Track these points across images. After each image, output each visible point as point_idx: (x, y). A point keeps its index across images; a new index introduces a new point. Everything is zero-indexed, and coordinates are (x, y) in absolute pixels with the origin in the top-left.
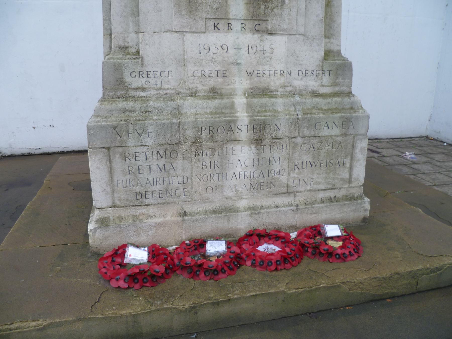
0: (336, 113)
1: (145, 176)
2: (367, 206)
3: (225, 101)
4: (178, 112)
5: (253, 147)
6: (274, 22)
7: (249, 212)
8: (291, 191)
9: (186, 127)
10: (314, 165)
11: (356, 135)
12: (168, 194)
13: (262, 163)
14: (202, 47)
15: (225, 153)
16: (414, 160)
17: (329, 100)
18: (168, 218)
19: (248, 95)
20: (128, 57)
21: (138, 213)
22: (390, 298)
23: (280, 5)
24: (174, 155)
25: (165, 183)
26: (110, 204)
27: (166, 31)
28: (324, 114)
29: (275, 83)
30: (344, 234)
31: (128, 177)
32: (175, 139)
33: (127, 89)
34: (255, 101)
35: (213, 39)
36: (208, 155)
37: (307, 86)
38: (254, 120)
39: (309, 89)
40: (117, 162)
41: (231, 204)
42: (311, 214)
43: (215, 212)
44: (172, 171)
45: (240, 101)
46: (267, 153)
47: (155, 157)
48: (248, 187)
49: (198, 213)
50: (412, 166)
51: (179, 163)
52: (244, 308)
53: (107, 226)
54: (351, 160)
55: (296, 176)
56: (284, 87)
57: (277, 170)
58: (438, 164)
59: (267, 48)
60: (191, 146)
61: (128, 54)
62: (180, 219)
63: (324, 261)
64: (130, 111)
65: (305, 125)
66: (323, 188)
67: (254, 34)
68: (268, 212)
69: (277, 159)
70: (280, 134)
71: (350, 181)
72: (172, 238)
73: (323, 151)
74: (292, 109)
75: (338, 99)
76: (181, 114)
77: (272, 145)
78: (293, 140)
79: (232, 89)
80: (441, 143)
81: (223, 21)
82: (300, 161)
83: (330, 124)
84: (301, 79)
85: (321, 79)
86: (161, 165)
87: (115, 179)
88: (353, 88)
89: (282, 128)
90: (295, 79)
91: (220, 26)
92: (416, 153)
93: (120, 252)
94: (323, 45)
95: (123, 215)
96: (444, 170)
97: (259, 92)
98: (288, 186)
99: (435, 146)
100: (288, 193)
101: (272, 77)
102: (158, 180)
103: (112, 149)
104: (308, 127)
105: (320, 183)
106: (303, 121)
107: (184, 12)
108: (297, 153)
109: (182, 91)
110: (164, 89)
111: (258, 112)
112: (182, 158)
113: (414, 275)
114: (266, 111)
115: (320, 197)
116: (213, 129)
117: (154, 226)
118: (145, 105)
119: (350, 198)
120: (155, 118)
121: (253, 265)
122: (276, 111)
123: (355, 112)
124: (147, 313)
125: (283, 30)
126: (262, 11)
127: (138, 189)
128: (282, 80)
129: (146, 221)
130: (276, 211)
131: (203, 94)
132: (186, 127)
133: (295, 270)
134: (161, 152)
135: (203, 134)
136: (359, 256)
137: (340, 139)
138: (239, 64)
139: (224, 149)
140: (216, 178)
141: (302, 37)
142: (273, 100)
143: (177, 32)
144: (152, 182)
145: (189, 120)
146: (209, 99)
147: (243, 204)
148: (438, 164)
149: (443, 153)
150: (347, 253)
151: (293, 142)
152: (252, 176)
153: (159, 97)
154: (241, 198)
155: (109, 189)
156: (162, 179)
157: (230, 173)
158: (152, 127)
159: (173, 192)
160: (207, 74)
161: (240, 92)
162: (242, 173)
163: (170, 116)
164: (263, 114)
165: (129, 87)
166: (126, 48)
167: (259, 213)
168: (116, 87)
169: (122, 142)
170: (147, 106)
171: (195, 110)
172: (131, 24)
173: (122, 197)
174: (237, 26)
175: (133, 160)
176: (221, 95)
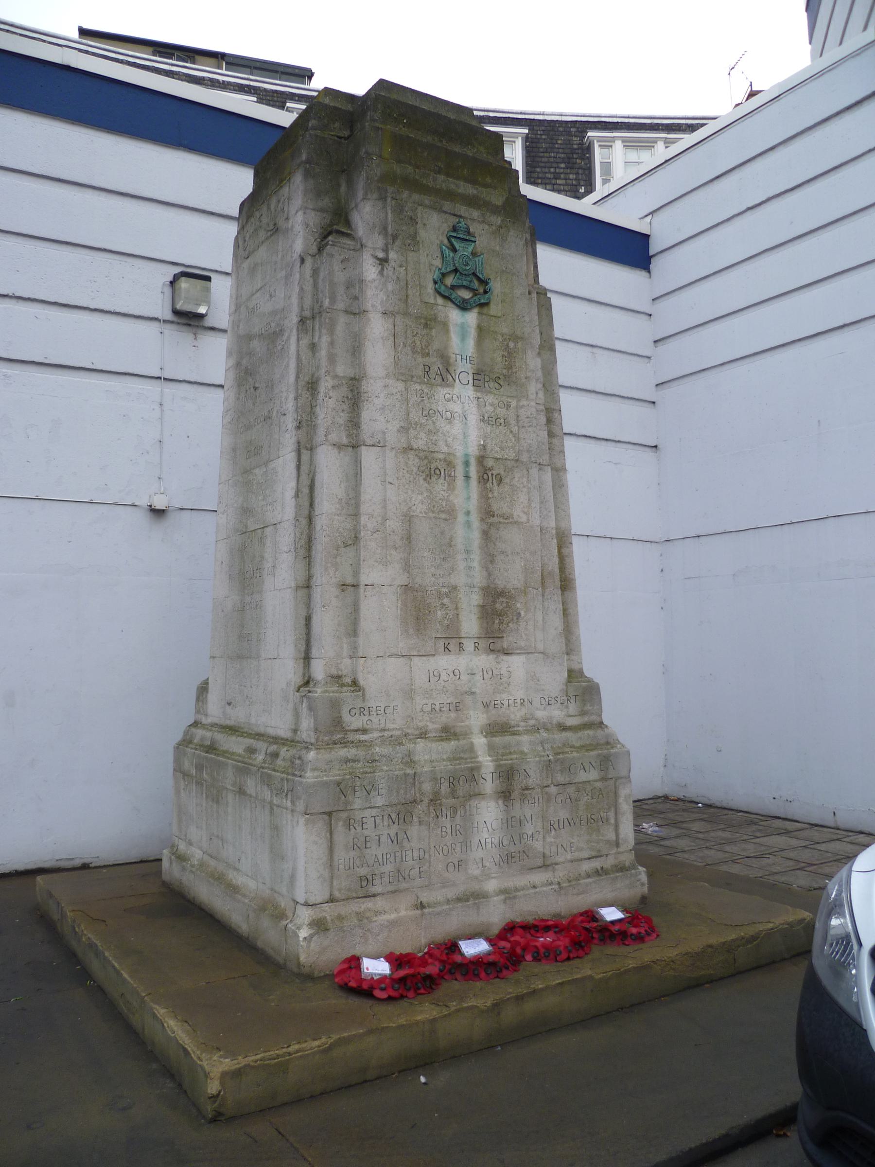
0: (592, 750)
1: (374, 851)
2: (644, 878)
3: (462, 742)
4: (409, 760)
5: (500, 802)
6: (510, 639)
7: (502, 897)
8: (548, 862)
9: (423, 779)
10: (572, 824)
11: (617, 779)
12: (401, 877)
13: (512, 824)
14: (431, 674)
15: (468, 813)
16: (660, 834)
17: (580, 734)
18: (403, 913)
19: (487, 733)
20: (345, 689)
21: (362, 910)
22: (707, 983)
23: (515, 618)
24: (408, 819)
25: (398, 860)
26: (327, 896)
27: (391, 656)
28: (578, 752)
29: (515, 715)
30: (628, 915)
31: (352, 854)
32: (409, 797)
33: (345, 732)
34: (497, 740)
35: (444, 663)
36: (449, 817)
37: (551, 717)
38: (500, 766)
39: (554, 722)
40: (341, 835)
41: (477, 887)
42: (578, 894)
43: (459, 900)
44: (405, 843)
45: (480, 741)
46: (517, 810)
47: (386, 823)
48: (497, 860)
49: (439, 904)
50: (662, 843)
51: (414, 831)
52: (551, 1002)
53: (327, 930)
54: (616, 814)
55: (553, 840)
56: (525, 720)
57: (530, 833)
58: (700, 836)
59: (504, 671)
60: (429, 805)
61: (343, 685)
62: (419, 912)
63: (619, 945)
64: (354, 761)
65: (558, 768)
66: (587, 856)
67: (488, 654)
68: (525, 895)
69: (528, 818)
70: (531, 782)
71: (617, 845)
72: (415, 940)
73: (582, 803)
74: (540, 748)
75: (590, 732)
76: (414, 762)
77: (523, 798)
78: (547, 789)
79: (467, 726)
80: (693, 805)
81: (454, 641)
82: (556, 819)
83: (587, 766)
84: (545, 709)
85: (567, 707)
86: (393, 835)
87: (336, 858)
88: (603, 716)
89: (532, 774)
90: (537, 709)
91: (451, 647)
92: (660, 822)
93: (354, 962)
94: (565, 664)
95: (343, 913)
96: (713, 843)
97: (498, 729)
98: (544, 856)
99: (684, 810)
100: (545, 866)
101: (512, 708)
102: (388, 856)
103: (334, 814)
104: (562, 771)
105: (581, 849)
106: (557, 763)
107: (411, 631)
108: (552, 808)
109: (409, 731)
110: (388, 730)
111: (503, 756)
112: (417, 823)
113: (728, 948)
114: (510, 753)
115: (584, 869)
116: (453, 780)
117: (387, 927)
118: (370, 752)
119: (621, 868)
120: (385, 768)
121: (537, 959)
122: (522, 752)
123: (612, 748)
124: (445, 1016)
125: (521, 648)
126: (496, 626)
127: (363, 871)
128: (524, 711)
129: (375, 919)
130: (535, 893)
131: (434, 734)
132: (423, 779)
133: (589, 957)
134: (394, 816)
135: (443, 788)
136: (658, 936)
137: (599, 784)
138: (473, 693)
139: (467, 807)
140: (458, 849)
141: (541, 656)
142: (517, 737)
143: (403, 656)
144: (381, 861)
145: (426, 769)
146: (442, 740)
147: (491, 886)
148: (700, 836)
149: (702, 820)
150: (643, 931)
151: (547, 793)
152: (501, 844)
153: (383, 741)
154: (489, 877)
155: (326, 874)
156: (393, 855)
157: (475, 841)
158: (383, 781)
159: (407, 873)
160: (437, 708)
161: (476, 730)
162: (489, 840)
163: (402, 766)
164: (509, 757)
165: (347, 728)
166: (339, 677)
167: (515, 897)
168: (332, 729)
169: (347, 803)
170: (373, 753)
171: (430, 755)
172: (345, 646)
173: (343, 884)
174: (469, 645)
175: (359, 829)
176: (455, 734)
